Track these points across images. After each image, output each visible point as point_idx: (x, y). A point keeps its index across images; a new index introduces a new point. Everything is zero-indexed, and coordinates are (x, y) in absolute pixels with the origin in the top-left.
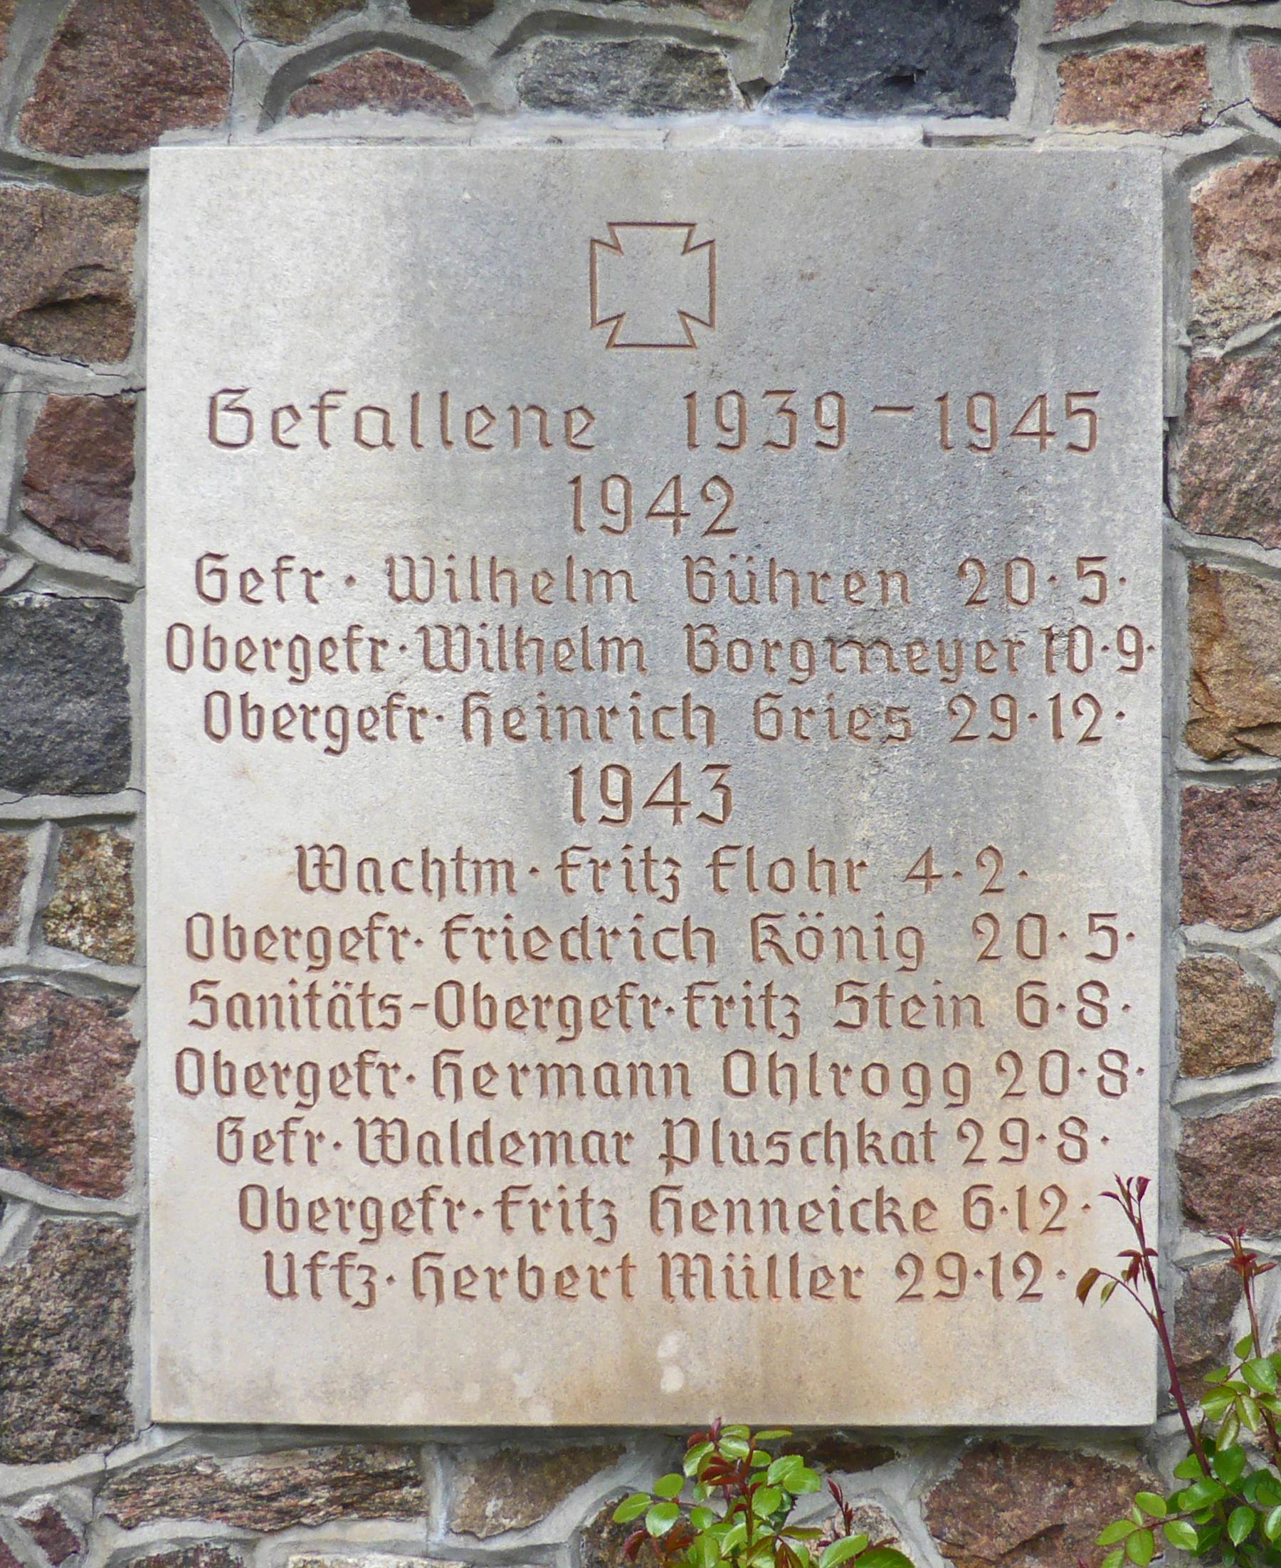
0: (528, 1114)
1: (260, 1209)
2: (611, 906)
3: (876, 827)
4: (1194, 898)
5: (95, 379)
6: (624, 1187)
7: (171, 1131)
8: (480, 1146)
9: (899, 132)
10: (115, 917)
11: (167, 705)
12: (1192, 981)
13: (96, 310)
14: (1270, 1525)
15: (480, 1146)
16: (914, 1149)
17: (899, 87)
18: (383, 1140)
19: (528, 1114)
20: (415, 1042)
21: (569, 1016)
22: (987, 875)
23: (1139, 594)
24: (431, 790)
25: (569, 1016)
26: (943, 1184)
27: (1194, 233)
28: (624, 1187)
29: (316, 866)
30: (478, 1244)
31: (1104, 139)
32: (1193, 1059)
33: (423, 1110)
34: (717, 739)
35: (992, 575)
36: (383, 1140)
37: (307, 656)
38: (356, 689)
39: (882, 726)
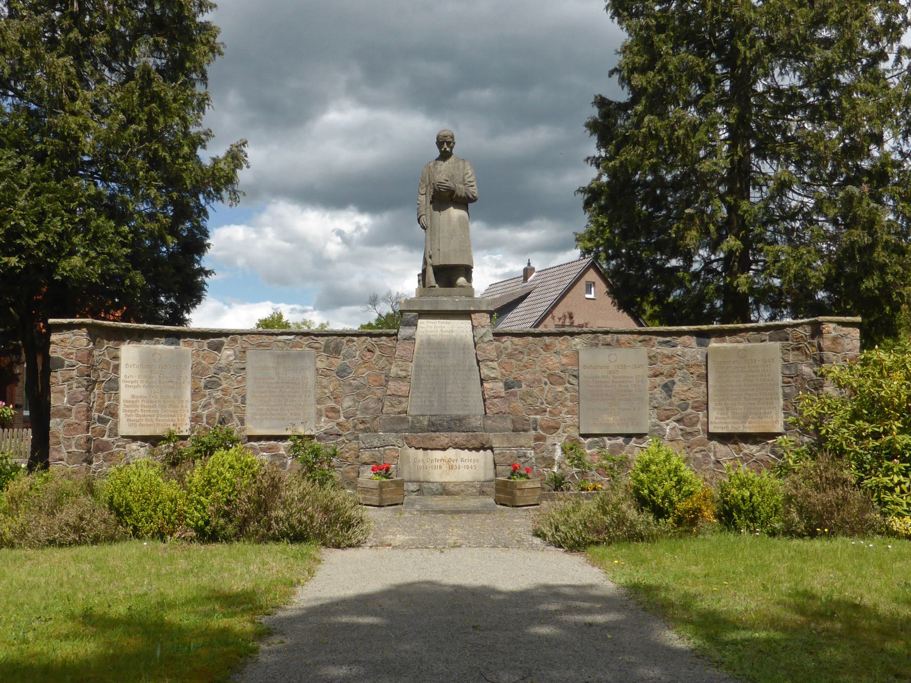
0: (148, 413)
1: (128, 420)
2: (153, 399)
3: (172, 394)
4: (192, 400)
5: (116, 363)
6: (154, 418)
7: (122, 415)
8: (144, 416)
9: (173, 347)
10: (117, 400)
11: (122, 385)
12: (192, 405)
13: (116, 358)
14: (908, 15)
15: (144, 416)
16: (174, 416)
17: (172, 344)
18: (137, 415)
19: (148, 413)
20: (140, 408)
21: (150, 407)
22: (179, 397)
23: (189, 379)
24: (141, 391)
25: (150, 407)
26: (176, 418)
27: (193, 355)
28: (154, 418)
29: (133, 396)
30: (144, 422)
31: (186, 348)
32: (193, 410)
33: (140, 413)
34: (714, 443)
35: (179, 377)
36: (137, 415)
37: (132, 382)
38: (136, 384)
39: (172, 388)
